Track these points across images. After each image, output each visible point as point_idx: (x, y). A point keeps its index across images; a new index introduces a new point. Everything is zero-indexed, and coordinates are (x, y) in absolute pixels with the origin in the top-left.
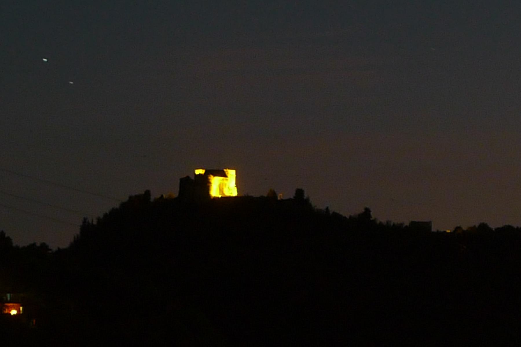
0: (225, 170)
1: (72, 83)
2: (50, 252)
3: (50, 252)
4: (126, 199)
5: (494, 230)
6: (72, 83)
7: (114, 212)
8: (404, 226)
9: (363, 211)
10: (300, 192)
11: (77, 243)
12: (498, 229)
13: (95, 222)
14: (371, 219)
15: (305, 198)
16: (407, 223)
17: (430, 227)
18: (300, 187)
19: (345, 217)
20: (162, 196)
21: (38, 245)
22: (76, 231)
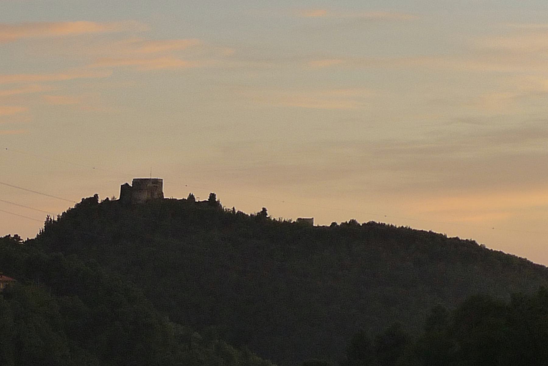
0: (99, 202)
1: (16, 240)
2: (21, 241)
3: (21, 241)
4: (80, 201)
5: (361, 225)
6: (16, 240)
7: (71, 211)
8: (292, 222)
9: (262, 210)
10: (213, 196)
11: (42, 236)
12: (364, 224)
13: (56, 219)
14: (267, 216)
15: (216, 200)
16: (295, 220)
17: (313, 223)
18: (16, 234)
19: (247, 215)
20: (10, 235)
21: (12, 236)
22: (43, 226)
